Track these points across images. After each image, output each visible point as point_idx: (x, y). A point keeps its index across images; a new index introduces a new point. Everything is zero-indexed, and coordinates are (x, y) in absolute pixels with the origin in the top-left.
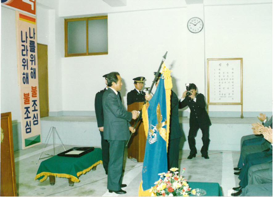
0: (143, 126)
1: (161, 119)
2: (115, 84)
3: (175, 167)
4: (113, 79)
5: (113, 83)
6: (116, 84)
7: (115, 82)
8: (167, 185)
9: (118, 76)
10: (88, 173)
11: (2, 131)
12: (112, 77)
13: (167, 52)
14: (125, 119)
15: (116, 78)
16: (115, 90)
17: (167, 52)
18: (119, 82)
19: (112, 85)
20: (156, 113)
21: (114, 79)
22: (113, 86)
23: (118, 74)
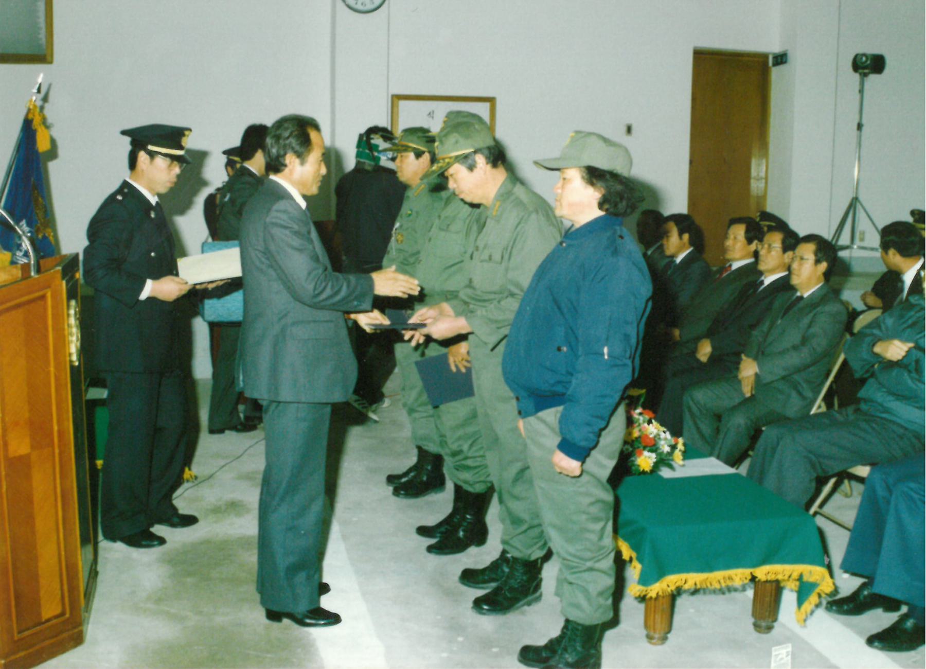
0: (900, 284)
1: (272, 146)
2: (297, 161)
3: (445, 122)
4: (290, 144)
5: (290, 159)
6: (302, 163)
7: (299, 155)
8: (490, 258)
9: (313, 135)
10: (341, 392)
11: (198, 287)
12: (286, 134)
13: (536, 163)
14: (333, 308)
15: (306, 142)
16: (299, 190)
17: (536, 163)
18: (314, 156)
19: (286, 166)
20: (635, 547)
21: (293, 142)
22: (287, 170)
23: (317, 127)
